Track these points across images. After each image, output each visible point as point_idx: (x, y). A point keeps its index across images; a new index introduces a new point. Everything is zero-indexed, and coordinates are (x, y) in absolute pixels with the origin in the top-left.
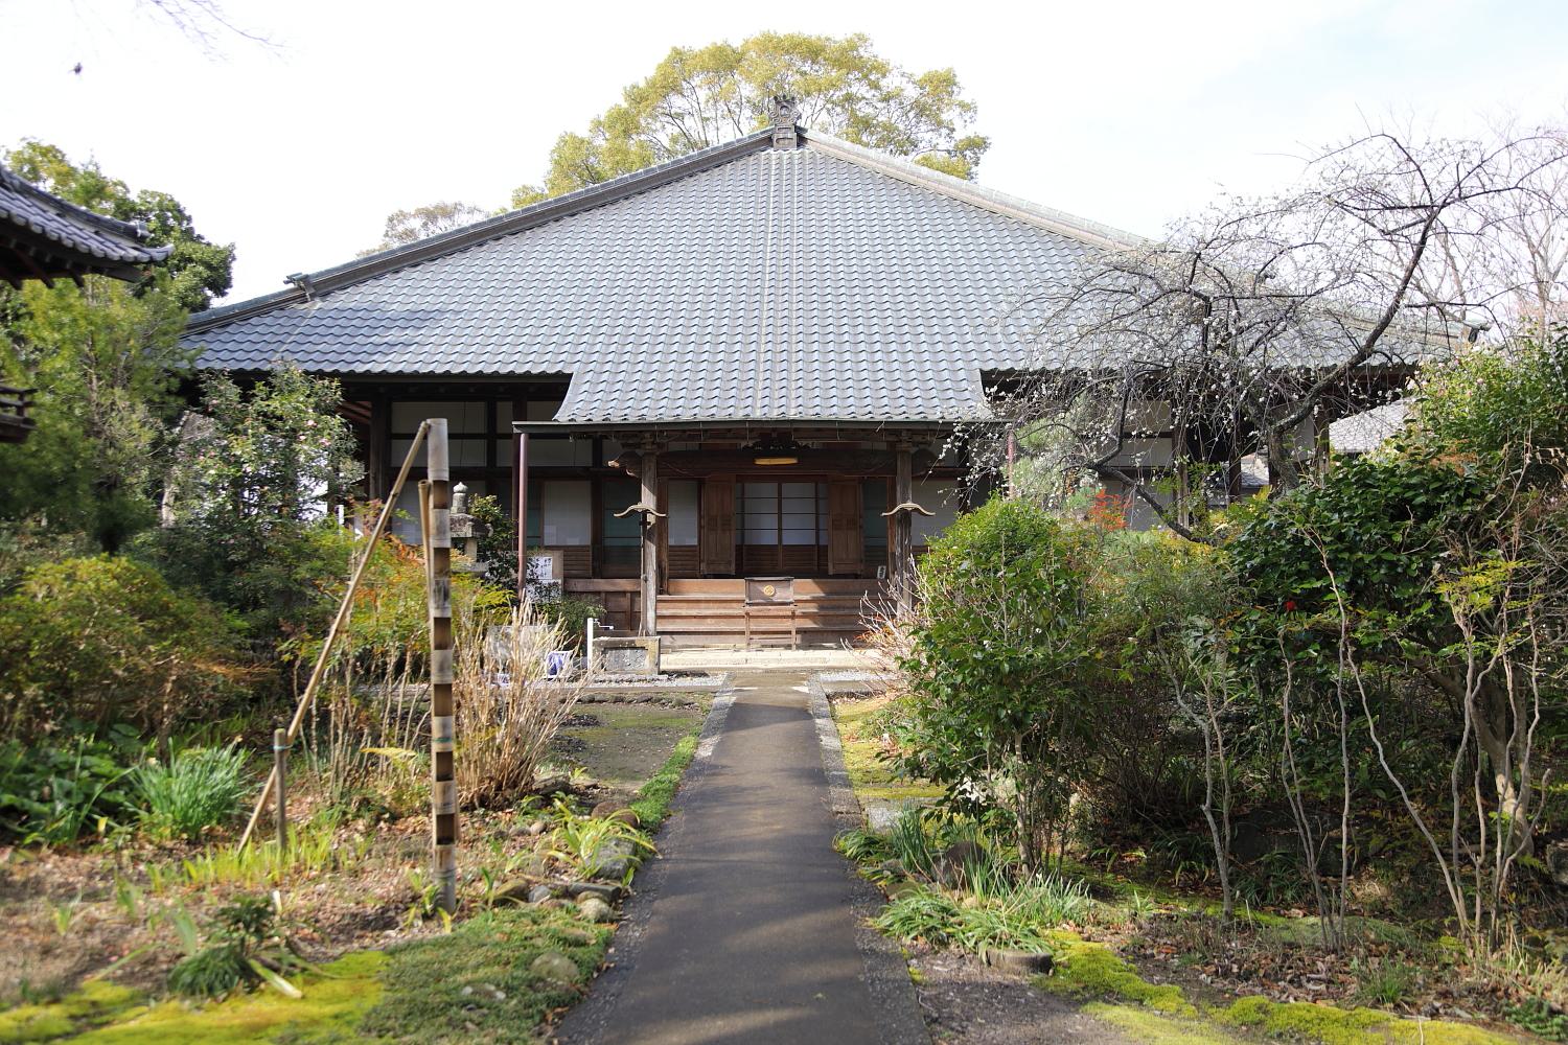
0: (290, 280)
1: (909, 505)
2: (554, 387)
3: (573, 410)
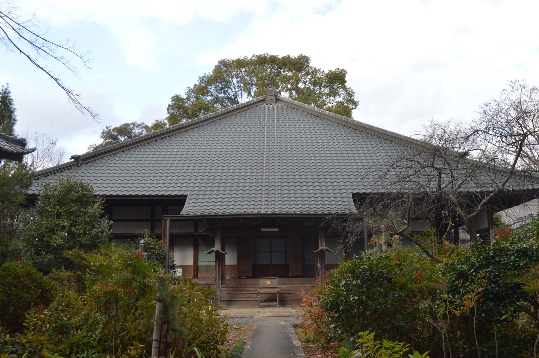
0: (73, 157)
1: (324, 248)
2: (180, 201)
3: (187, 210)
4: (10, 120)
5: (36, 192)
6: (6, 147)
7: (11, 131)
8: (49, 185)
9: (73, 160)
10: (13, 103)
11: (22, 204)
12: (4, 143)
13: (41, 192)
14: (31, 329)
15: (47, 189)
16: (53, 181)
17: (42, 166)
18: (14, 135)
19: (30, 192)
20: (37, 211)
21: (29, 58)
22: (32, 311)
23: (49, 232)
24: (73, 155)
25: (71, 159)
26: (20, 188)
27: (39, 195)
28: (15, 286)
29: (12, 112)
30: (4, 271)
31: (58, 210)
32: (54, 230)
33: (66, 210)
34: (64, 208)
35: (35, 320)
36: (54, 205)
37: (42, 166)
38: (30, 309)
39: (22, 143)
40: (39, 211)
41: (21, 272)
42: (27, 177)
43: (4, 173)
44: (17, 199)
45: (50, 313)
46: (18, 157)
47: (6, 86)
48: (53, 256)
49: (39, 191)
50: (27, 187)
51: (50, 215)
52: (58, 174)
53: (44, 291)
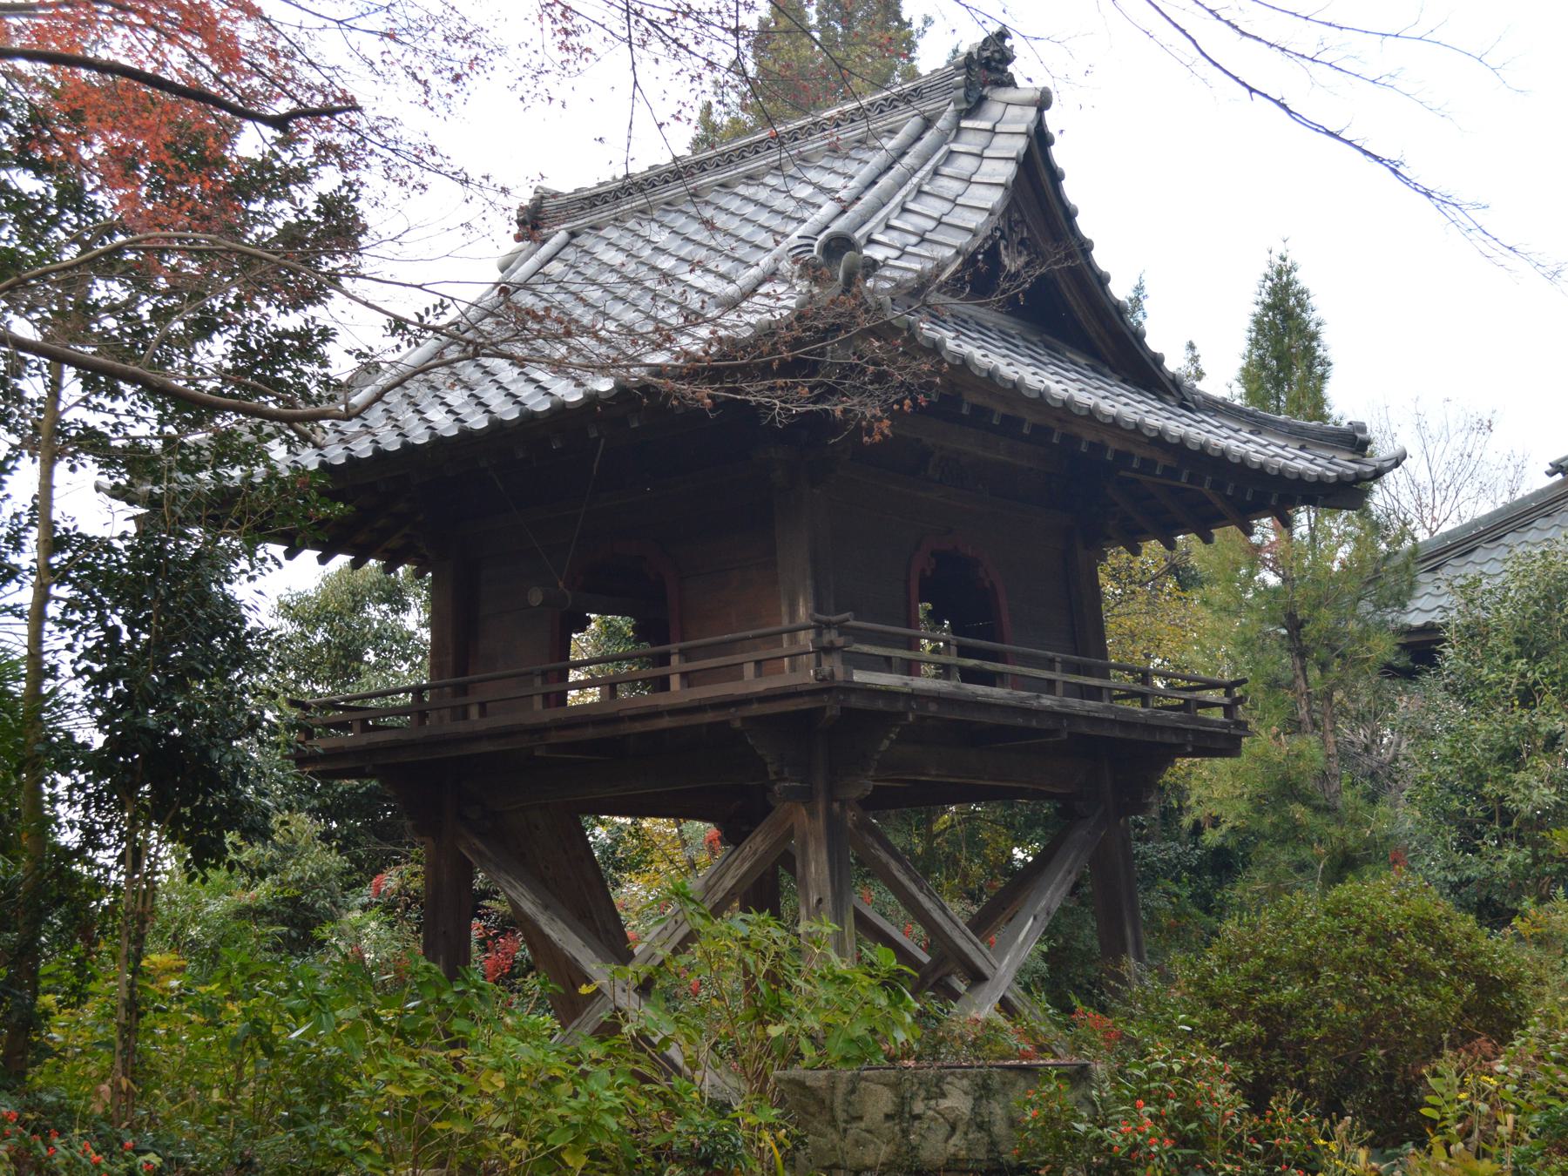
0: (1557, 468)
4: (1310, 367)
5: (1437, 617)
6: (1300, 465)
7: (1318, 404)
8: (1476, 582)
9: (1559, 476)
10: (1312, 302)
11: (1389, 666)
12: (1292, 450)
13: (1453, 613)
14: (1453, 1131)
15: (1472, 601)
16: (1492, 567)
17: (1454, 517)
18: (1329, 417)
19: (1416, 620)
20: (1446, 687)
21: (1284, 106)
22: (1448, 1063)
23: (1501, 759)
24: (1555, 457)
25: (1550, 474)
26: (1378, 607)
27: (1446, 625)
28: (1380, 969)
29: (1314, 336)
30: (1335, 916)
31: (1523, 675)
32: (1517, 753)
33: (1553, 673)
34: (1545, 665)
35: (1462, 1096)
36: (1508, 659)
37: (1454, 517)
38: (1440, 1056)
39: (1354, 441)
40: (1454, 685)
41: (1395, 915)
42: (1396, 568)
43: (1315, 561)
44: (1369, 650)
45: (1519, 1070)
46: (1346, 493)
47: (1279, 249)
48: (1527, 850)
49: (1445, 610)
50: (1401, 600)
51: (1496, 698)
52: (1508, 539)
53: (1489, 985)
